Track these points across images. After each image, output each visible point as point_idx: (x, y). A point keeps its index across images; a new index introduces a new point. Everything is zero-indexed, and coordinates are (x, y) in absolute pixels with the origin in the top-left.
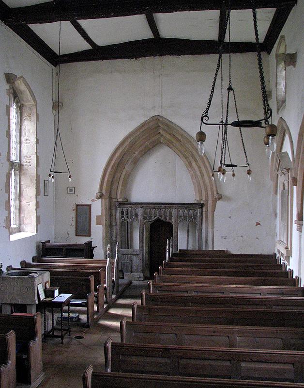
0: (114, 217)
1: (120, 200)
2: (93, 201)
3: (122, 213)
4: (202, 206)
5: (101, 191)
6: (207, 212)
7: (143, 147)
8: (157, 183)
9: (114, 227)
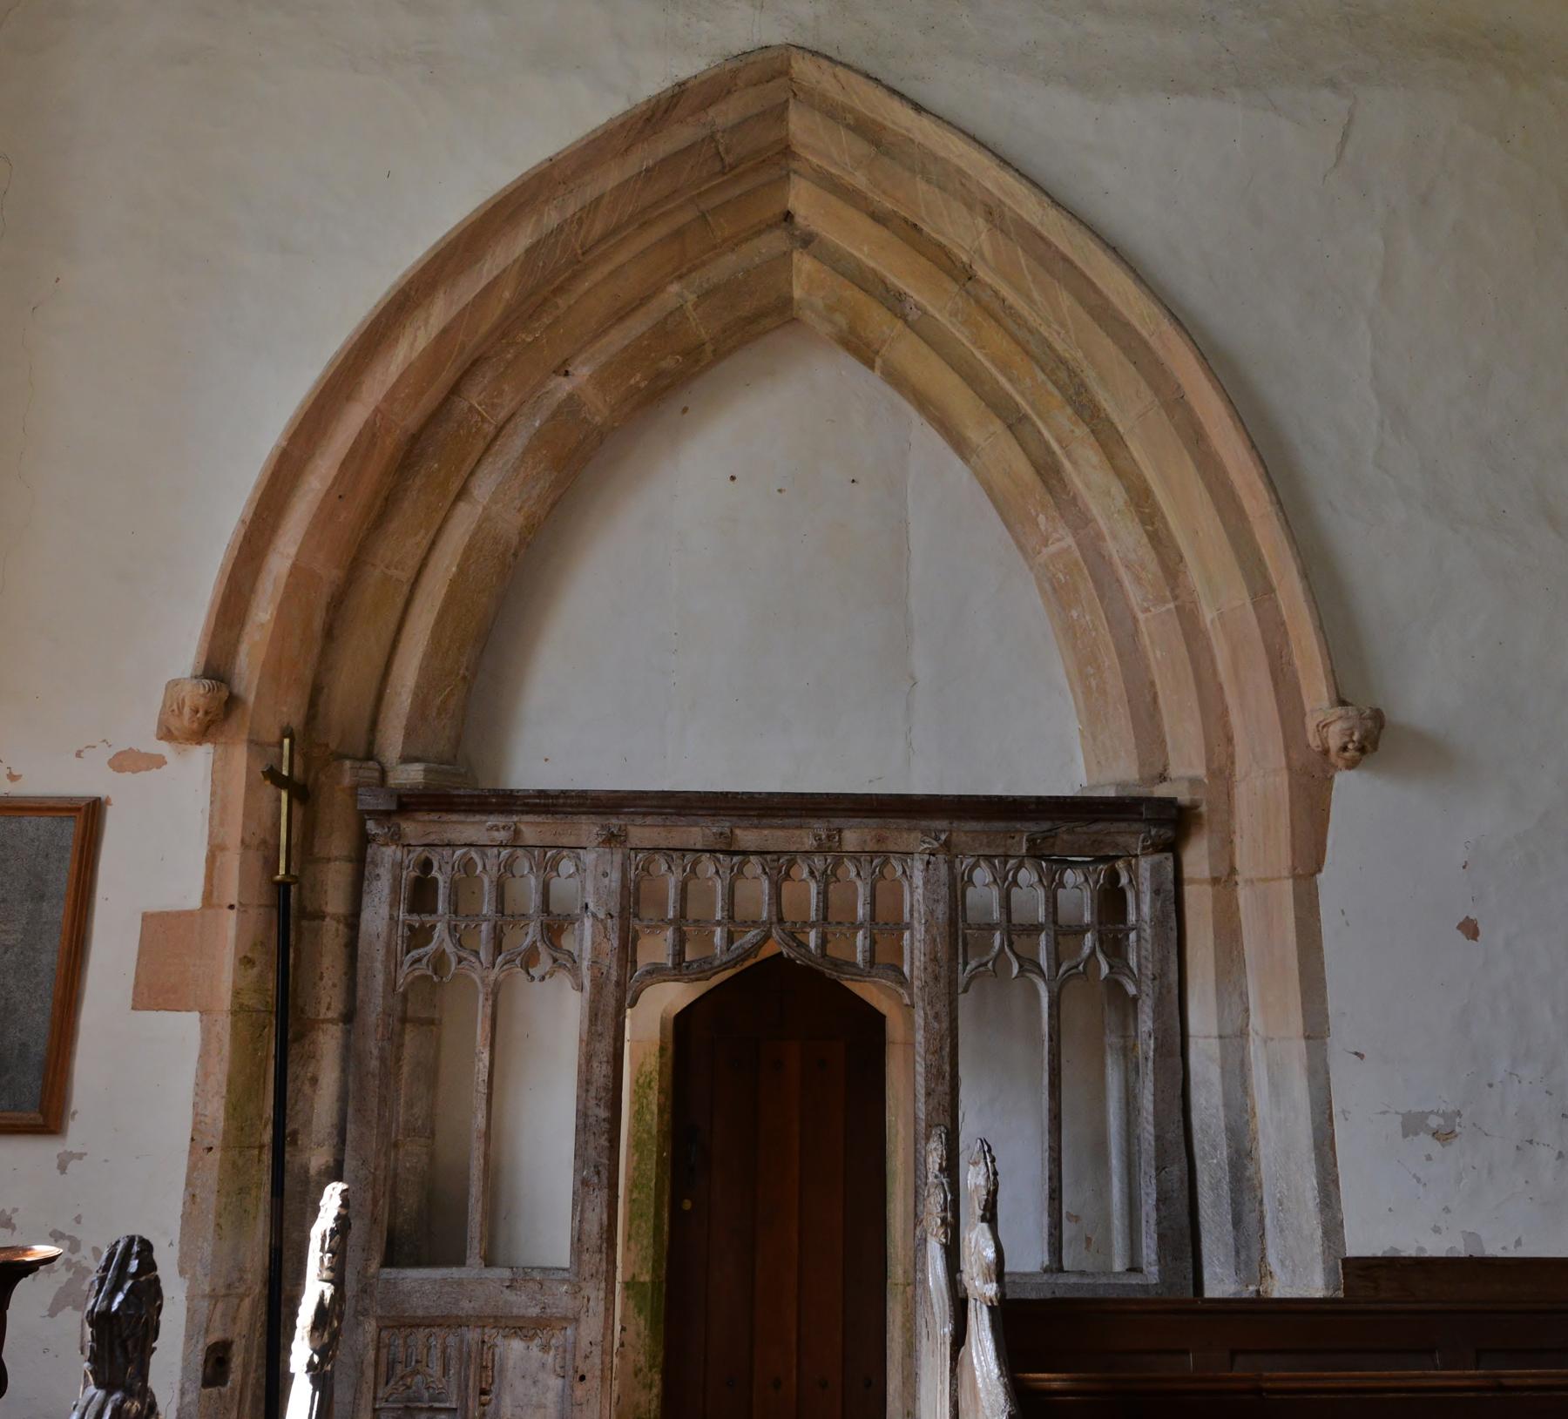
0: (331, 935)
1: (411, 775)
2: (127, 761)
3: (421, 894)
4: (1171, 823)
5: (216, 670)
6: (1225, 880)
7: (638, 325)
8: (759, 622)
9: (329, 1042)
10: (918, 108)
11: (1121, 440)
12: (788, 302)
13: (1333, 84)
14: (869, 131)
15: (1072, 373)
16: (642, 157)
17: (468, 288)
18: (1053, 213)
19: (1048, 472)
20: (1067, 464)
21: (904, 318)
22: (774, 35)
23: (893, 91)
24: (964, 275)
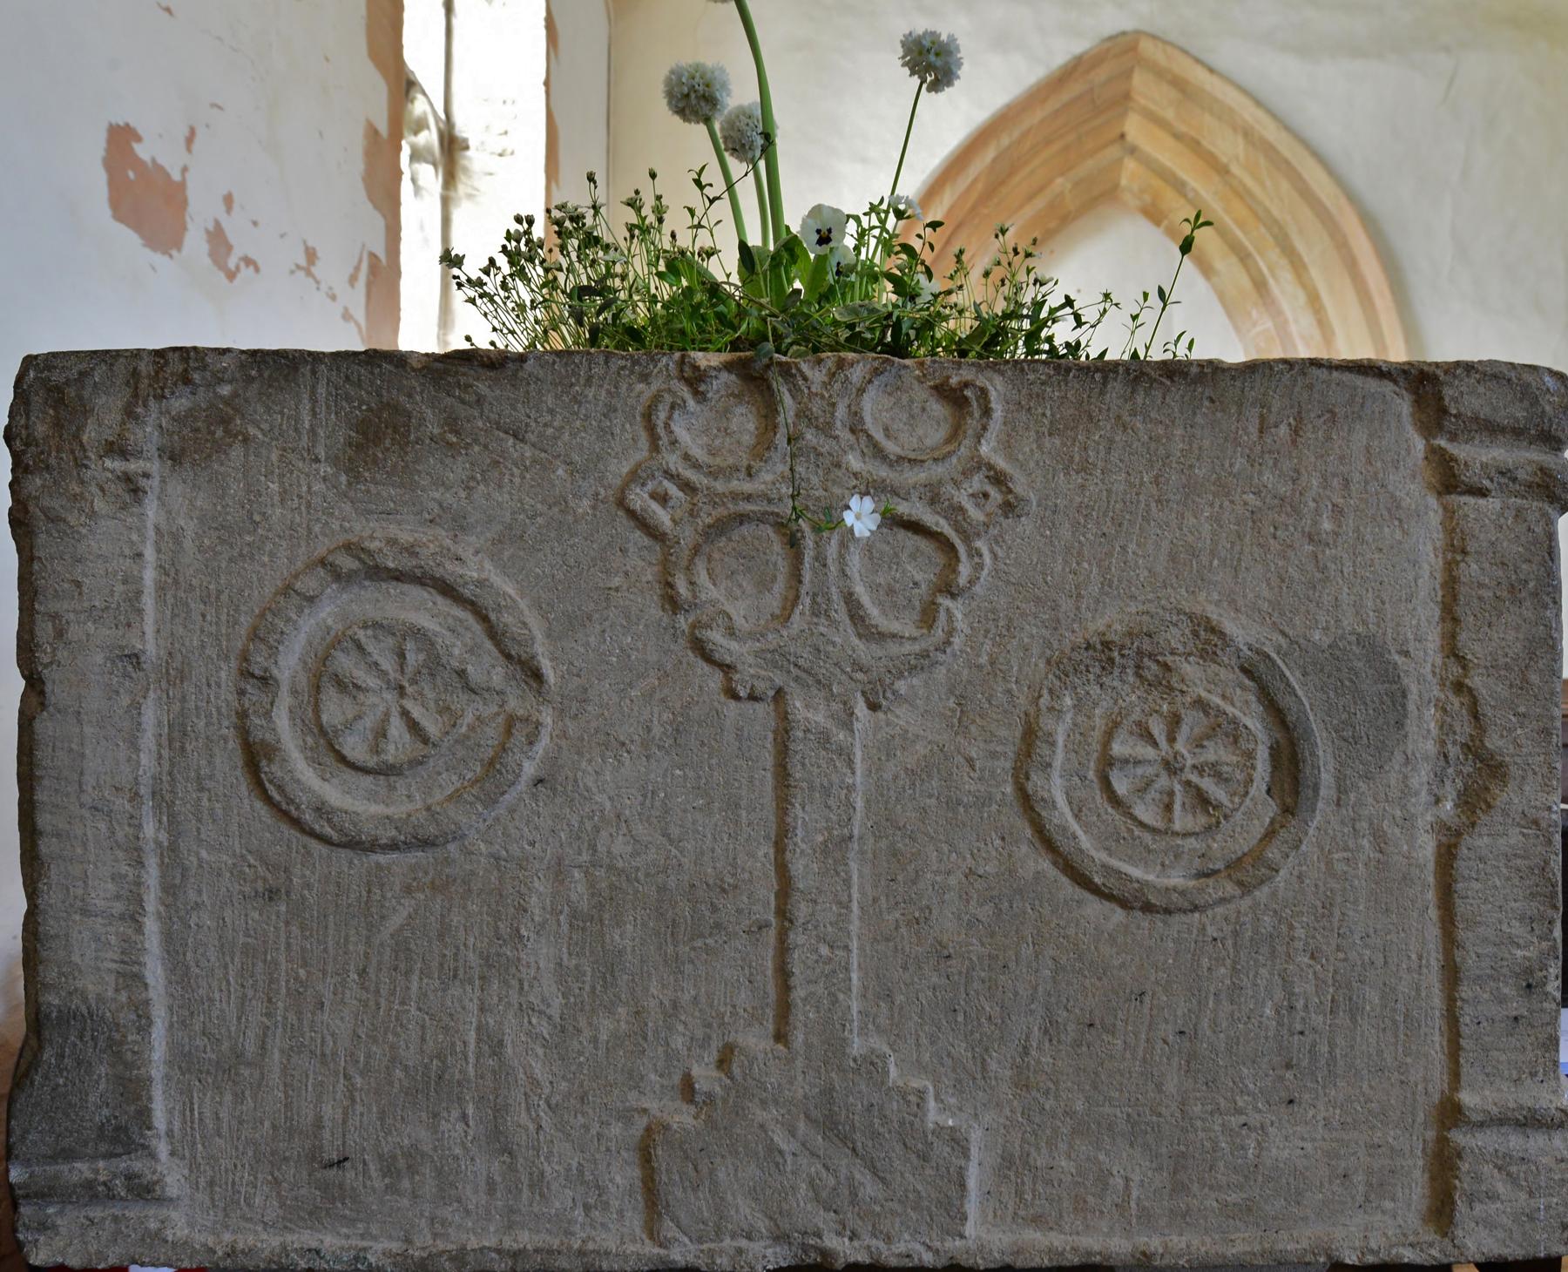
7: (1040, 203)
10: (1211, 70)
11: (1304, 266)
12: (1116, 187)
13: (1447, 49)
14: (1179, 84)
15: (1281, 228)
16: (1053, 104)
17: (963, 183)
18: (1284, 134)
19: (1260, 285)
20: (1271, 281)
21: (1185, 196)
22: (1125, 23)
23: (1198, 61)
24: (1223, 171)
